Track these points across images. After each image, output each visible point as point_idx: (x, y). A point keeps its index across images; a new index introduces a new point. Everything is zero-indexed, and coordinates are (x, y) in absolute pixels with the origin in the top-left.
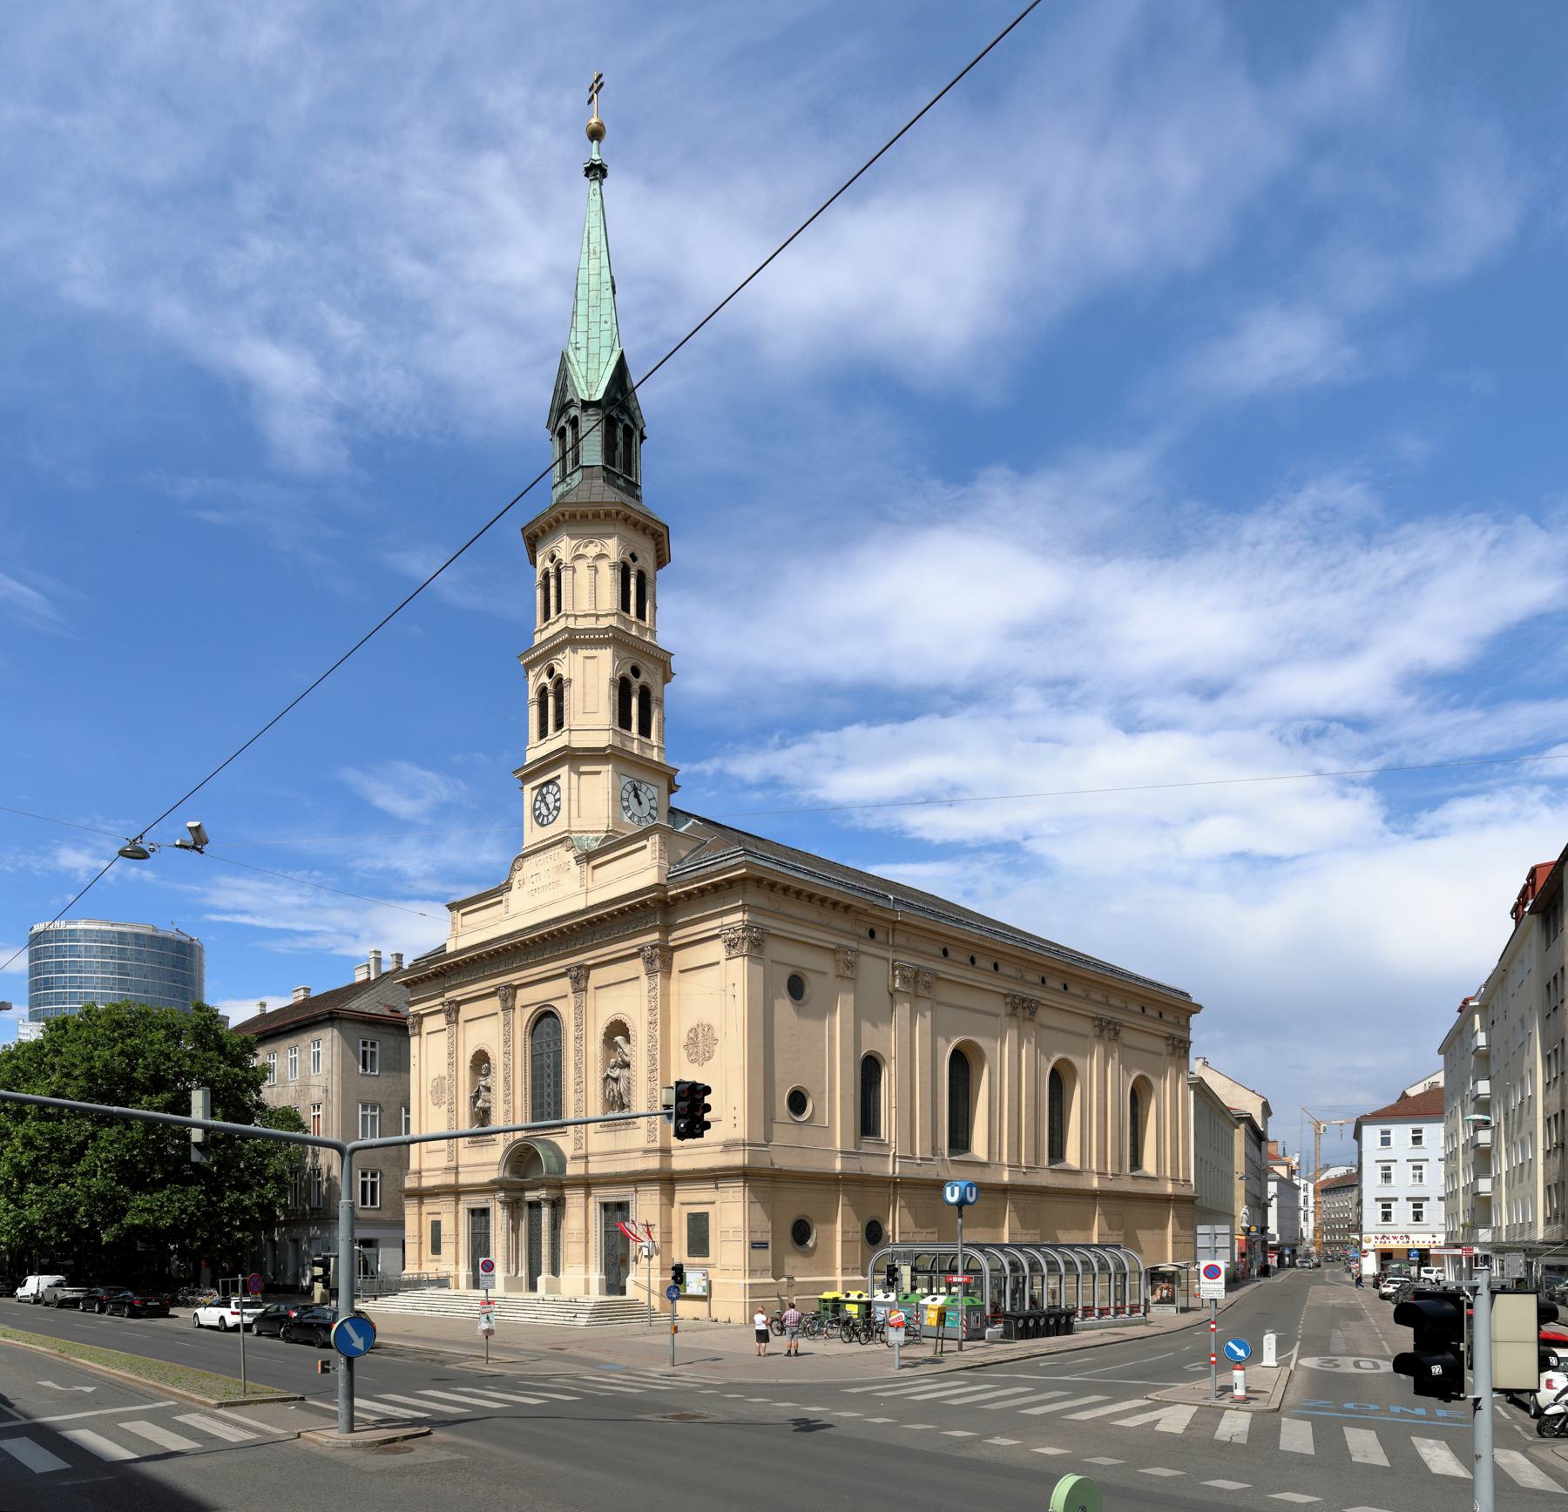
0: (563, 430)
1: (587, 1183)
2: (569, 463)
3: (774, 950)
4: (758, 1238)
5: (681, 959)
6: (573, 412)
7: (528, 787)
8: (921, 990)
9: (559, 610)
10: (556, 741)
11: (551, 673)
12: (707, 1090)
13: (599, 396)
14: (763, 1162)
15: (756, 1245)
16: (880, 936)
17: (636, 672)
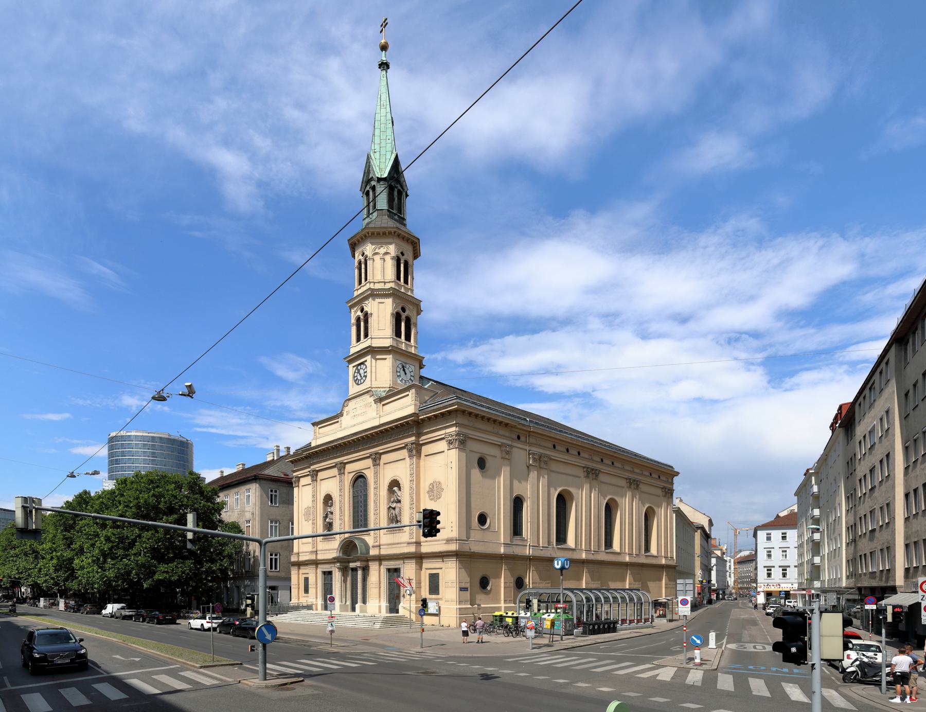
0: (368, 192)
1: (380, 559)
2: (371, 208)
3: (471, 445)
4: (463, 585)
5: (425, 450)
6: (373, 183)
7: (351, 366)
8: (542, 465)
9: (366, 279)
10: (365, 343)
11: (362, 310)
12: (438, 514)
13: (385, 175)
14: (466, 549)
15: (462, 589)
16: (522, 438)
17: (403, 310)
